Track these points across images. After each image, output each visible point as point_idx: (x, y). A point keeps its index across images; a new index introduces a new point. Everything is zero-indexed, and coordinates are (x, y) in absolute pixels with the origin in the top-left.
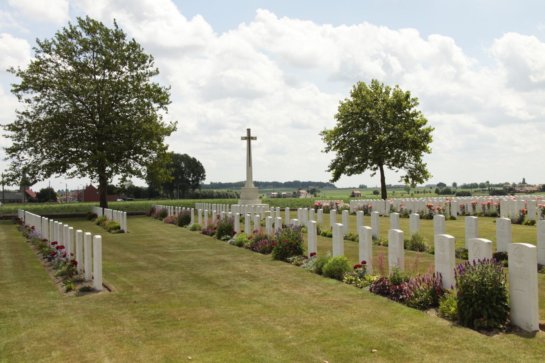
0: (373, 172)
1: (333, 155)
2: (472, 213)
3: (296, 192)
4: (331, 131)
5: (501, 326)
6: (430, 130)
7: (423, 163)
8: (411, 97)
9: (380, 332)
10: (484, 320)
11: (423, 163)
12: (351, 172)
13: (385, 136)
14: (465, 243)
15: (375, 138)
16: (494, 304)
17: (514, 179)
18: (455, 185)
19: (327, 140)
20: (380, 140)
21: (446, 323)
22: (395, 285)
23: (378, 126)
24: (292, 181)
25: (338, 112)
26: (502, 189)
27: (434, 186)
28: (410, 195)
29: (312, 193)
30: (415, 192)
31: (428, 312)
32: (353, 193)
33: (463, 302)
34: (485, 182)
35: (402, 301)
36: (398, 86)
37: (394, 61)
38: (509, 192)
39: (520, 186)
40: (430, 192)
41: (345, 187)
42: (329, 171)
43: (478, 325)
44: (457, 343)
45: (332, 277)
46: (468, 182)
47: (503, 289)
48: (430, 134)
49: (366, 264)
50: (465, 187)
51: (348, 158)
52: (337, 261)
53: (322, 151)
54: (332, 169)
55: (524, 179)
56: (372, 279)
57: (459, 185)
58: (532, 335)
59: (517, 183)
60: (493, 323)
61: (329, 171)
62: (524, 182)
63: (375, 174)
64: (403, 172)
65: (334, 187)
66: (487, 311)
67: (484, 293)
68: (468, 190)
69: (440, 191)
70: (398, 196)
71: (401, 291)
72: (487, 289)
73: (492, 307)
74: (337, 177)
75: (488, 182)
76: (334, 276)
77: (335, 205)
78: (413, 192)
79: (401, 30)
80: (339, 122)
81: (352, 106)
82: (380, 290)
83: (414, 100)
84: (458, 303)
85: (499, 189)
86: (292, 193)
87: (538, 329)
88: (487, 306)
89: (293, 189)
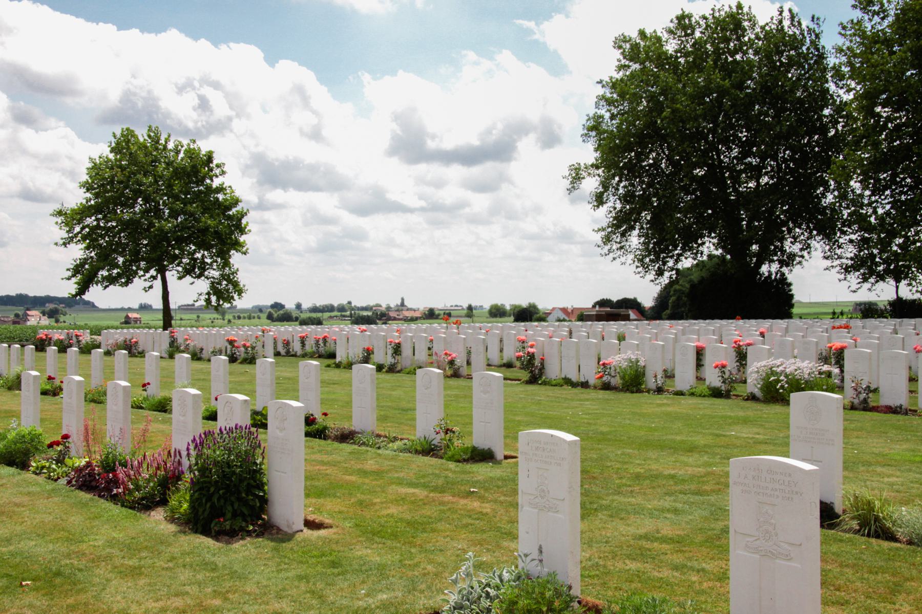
0: (148, 284)
1: (77, 251)
2: (299, 352)
3: (20, 313)
4: (73, 210)
5: (251, 528)
6: (243, 215)
7: (235, 267)
8: (215, 162)
9: (51, 552)
10: (225, 521)
11: (235, 267)
12: (111, 280)
13: (169, 222)
14: (845, 430)
15: (151, 225)
16: (244, 495)
17: (387, 300)
18: (299, 306)
19: (67, 225)
20: (161, 229)
21: (173, 528)
22: (108, 472)
23: (159, 205)
24: (13, 293)
25: (87, 177)
26: (370, 314)
27: (266, 307)
28: (226, 321)
29: (50, 316)
30: (234, 317)
31: (153, 513)
32: (127, 317)
33: (196, 494)
34: (345, 302)
35: (114, 498)
36: (194, 142)
37: (216, 100)
38: (380, 319)
39: (398, 310)
40: (259, 318)
41: (113, 307)
42: (69, 279)
43: (216, 529)
44: (172, 559)
45: (10, 463)
46: (320, 303)
47: (259, 472)
48: (244, 221)
49: (70, 440)
50: (315, 309)
51: (105, 258)
52: (24, 436)
53: (56, 244)
54: (74, 276)
55: (403, 300)
56: (76, 465)
57: (305, 306)
58: (288, 537)
59: (392, 306)
60: (240, 523)
61: (69, 279)
62: (403, 304)
63: (151, 287)
64: (203, 285)
65: (91, 306)
66: (232, 505)
67: (230, 479)
68: (319, 315)
69: (275, 315)
70: (204, 323)
71: (116, 482)
72: (234, 473)
73: (240, 499)
74: (84, 287)
75: (350, 303)
76: (14, 461)
77: (74, 338)
78: (231, 317)
79: (232, 45)
80: (88, 195)
81: (112, 168)
82: (85, 481)
83: (218, 166)
84: (191, 496)
85: (365, 313)
86: (12, 317)
87: (302, 527)
88: (233, 499)
89: (14, 308)
